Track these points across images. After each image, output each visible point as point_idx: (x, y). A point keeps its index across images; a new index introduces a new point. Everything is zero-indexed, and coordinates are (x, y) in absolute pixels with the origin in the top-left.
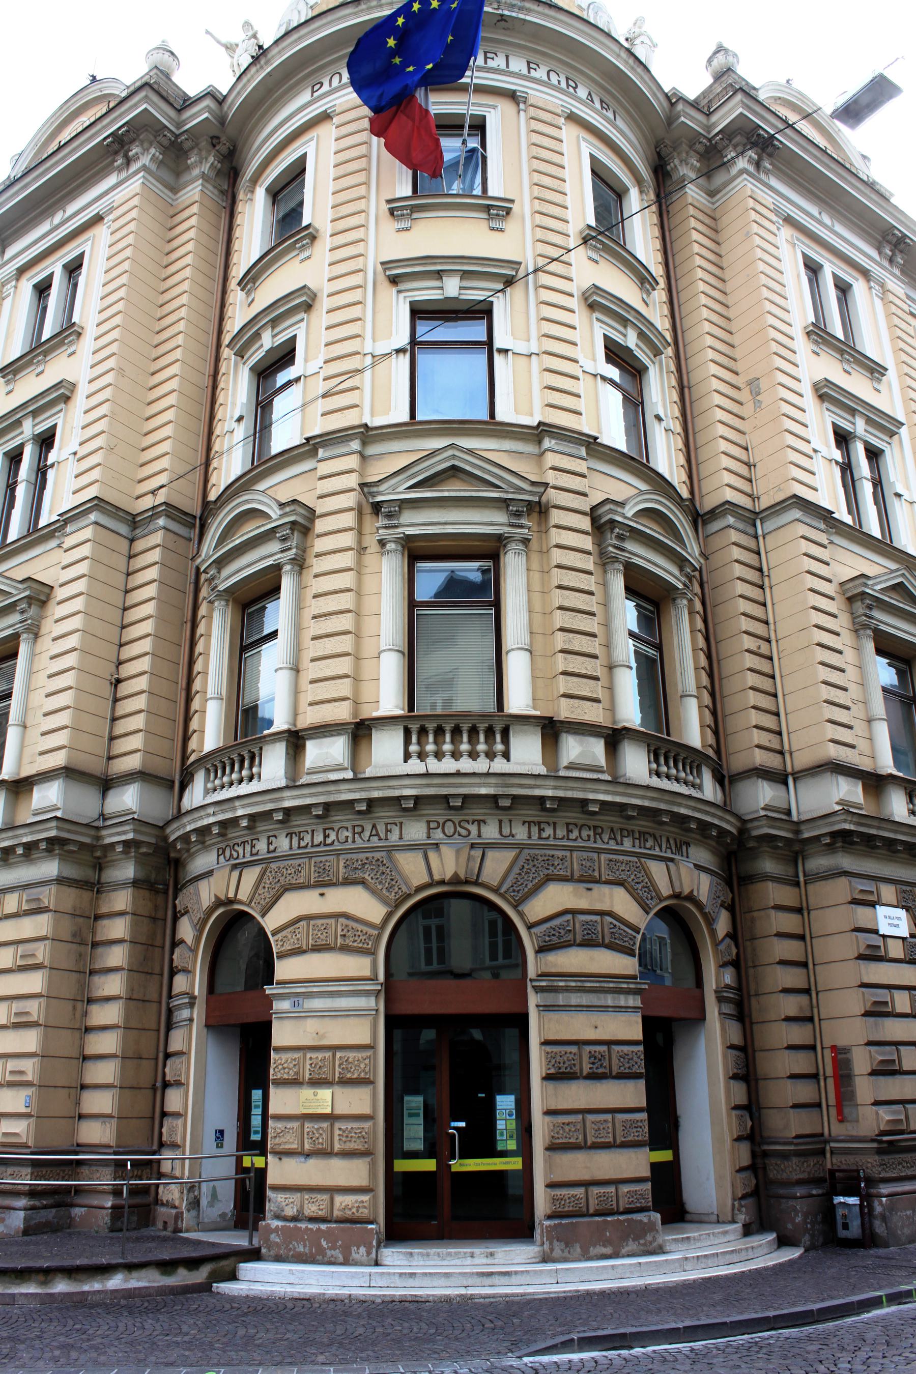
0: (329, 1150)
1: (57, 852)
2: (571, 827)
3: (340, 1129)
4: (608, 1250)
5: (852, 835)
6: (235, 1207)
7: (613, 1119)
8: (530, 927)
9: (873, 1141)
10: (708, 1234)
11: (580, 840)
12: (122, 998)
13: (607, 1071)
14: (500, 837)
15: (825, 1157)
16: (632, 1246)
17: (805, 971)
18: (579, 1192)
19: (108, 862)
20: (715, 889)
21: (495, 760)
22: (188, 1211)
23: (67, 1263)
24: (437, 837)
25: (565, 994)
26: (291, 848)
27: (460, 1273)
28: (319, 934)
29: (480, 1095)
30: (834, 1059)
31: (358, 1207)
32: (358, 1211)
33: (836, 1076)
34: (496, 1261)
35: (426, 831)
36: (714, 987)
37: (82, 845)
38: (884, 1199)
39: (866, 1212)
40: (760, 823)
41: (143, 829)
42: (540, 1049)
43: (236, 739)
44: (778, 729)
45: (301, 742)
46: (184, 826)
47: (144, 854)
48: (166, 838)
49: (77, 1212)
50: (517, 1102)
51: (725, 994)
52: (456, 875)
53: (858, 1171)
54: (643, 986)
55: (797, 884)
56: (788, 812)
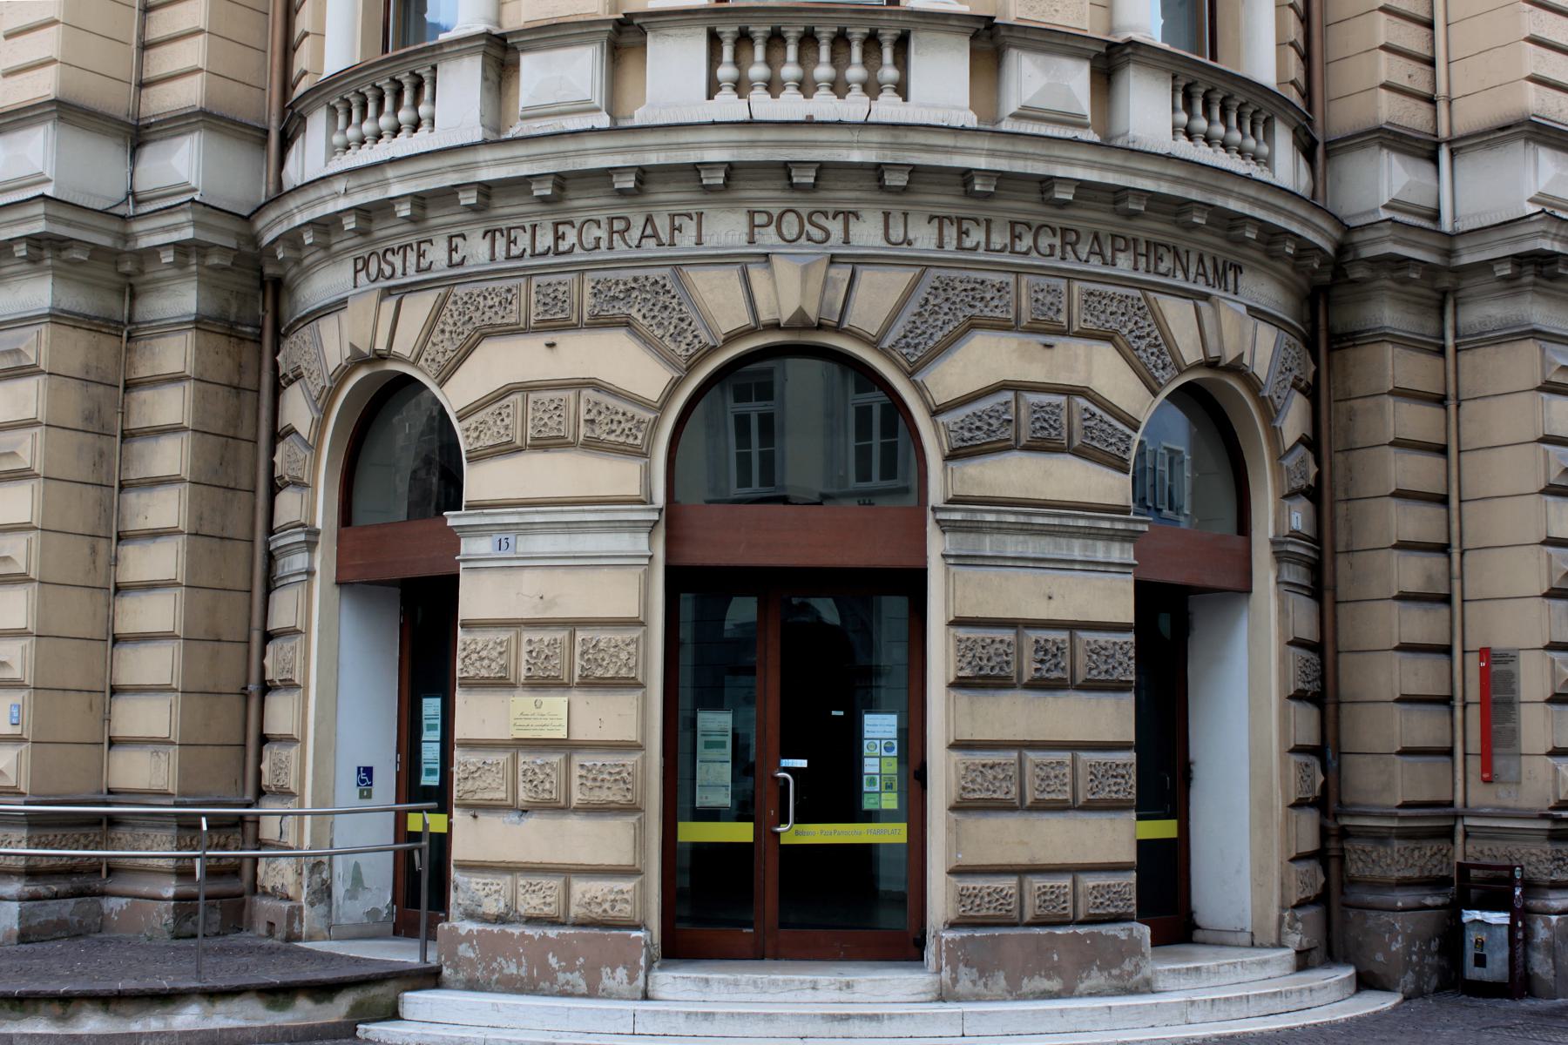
0: (563, 803)
1: (49, 262)
2: (1018, 229)
3: (582, 766)
4: (1055, 985)
5: (1556, 262)
6: (394, 901)
7: (1074, 761)
8: (935, 412)
9: (1543, 817)
10: (1234, 965)
11: (1034, 254)
12: (181, 533)
13: (1067, 676)
14: (884, 244)
15: (1453, 842)
16: (1097, 979)
17: (1443, 511)
18: (1008, 884)
19: (148, 282)
20: (1283, 354)
21: (881, 98)
22: (312, 905)
23: (101, 986)
24: (769, 242)
25: (997, 537)
26: (493, 259)
27: (792, 1015)
28: (546, 417)
29: (834, 713)
30: (1485, 673)
31: (615, 901)
32: (613, 908)
33: (1486, 703)
34: (856, 997)
35: (746, 230)
36: (1271, 534)
37: (96, 250)
38: (1554, 918)
39: (1519, 939)
40: (1380, 234)
41: (213, 220)
42: (947, 632)
43: (385, 50)
44: (1428, 53)
45: (510, 57)
46: (290, 215)
47: (213, 268)
48: (254, 239)
49: (113, 905)
50: (904, 733)
51: (1291, 548)
52: (801, 312)
53: (1512, 868)
54: (1140, 527)
55: (1441, 351)
56: (1436, 216)
